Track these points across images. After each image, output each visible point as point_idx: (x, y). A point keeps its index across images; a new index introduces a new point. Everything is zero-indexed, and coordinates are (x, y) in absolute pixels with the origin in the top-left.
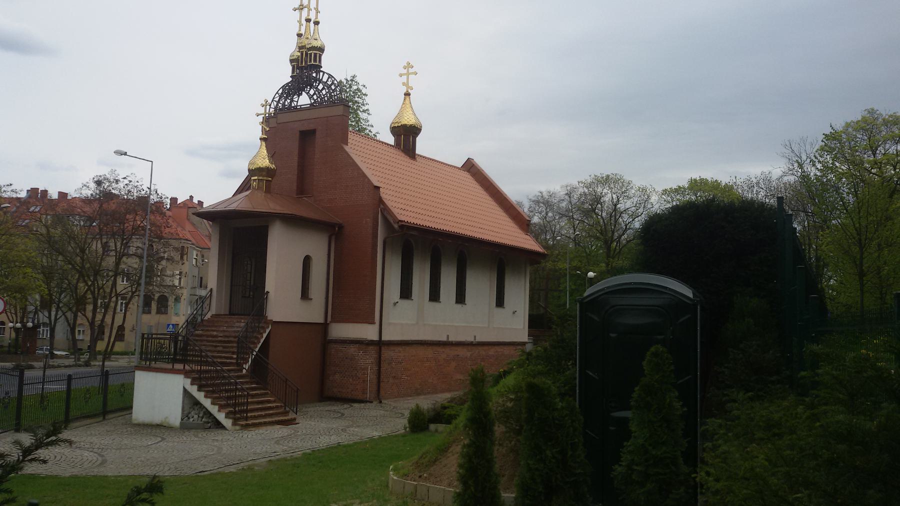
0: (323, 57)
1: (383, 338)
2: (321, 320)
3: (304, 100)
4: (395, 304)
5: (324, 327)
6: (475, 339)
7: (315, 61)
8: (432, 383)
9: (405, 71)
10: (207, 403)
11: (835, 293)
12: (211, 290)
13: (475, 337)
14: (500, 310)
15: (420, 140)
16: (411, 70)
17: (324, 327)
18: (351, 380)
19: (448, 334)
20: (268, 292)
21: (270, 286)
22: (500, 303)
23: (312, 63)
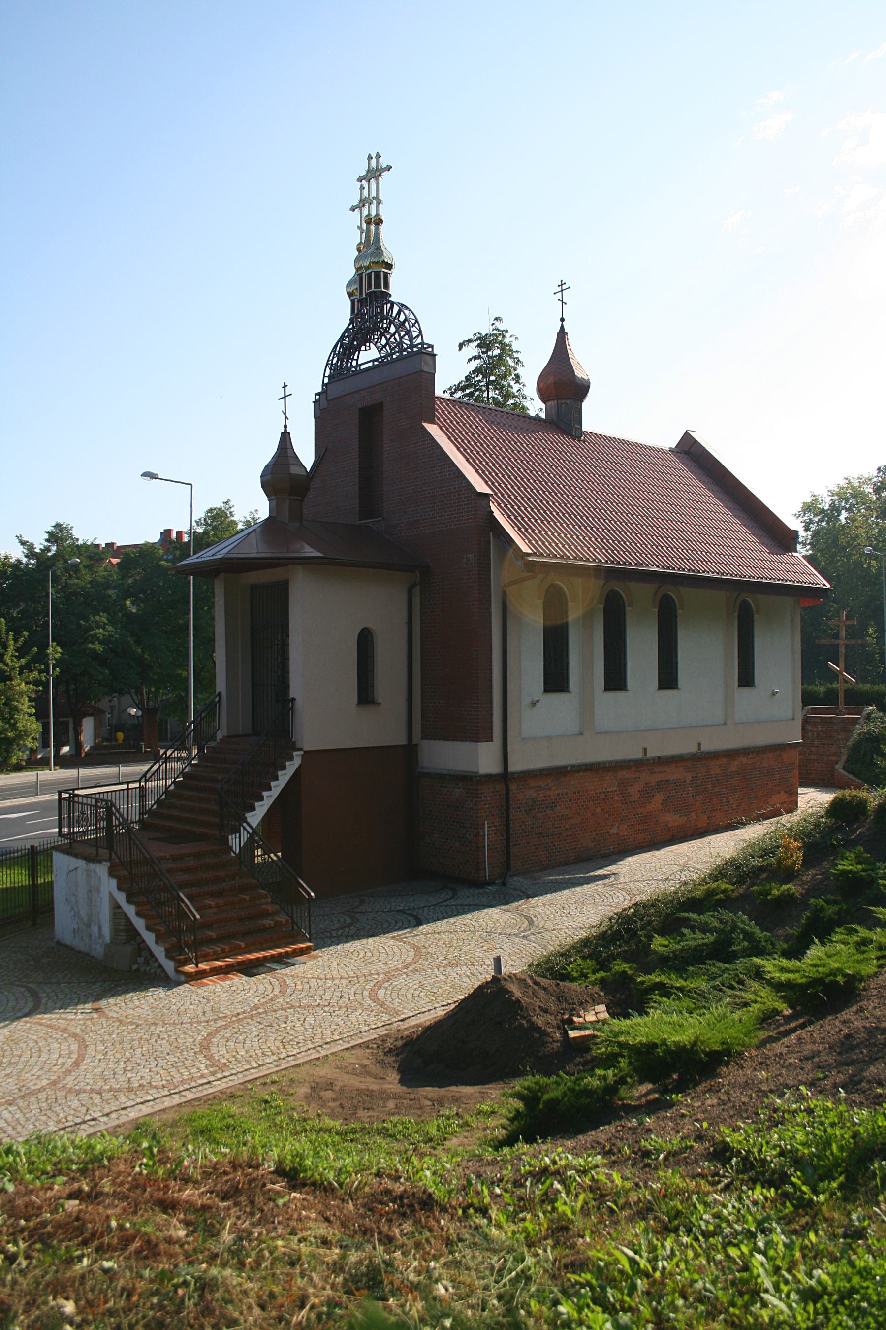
0: (391, 280)
1: (511, 769)
2: (402, 740)
3: (368, 355)
4: (534, 704)
5: (409, 751)
6: (699, 749)
7: (378, 285)
8: (618, 834)
9: (560, 289)
10: (139, 924)
11: (705, 1125)
12: (220, 694)
13: (699, 745)
14: (746, 691)
15: (587, 406)
16: (564, 286)
17: (409, 751)
18: (457, 844)
19: (645, 745)
20: (293, 700)
21: (296, 690)
22: (746, 679)
23: (373, 289)
